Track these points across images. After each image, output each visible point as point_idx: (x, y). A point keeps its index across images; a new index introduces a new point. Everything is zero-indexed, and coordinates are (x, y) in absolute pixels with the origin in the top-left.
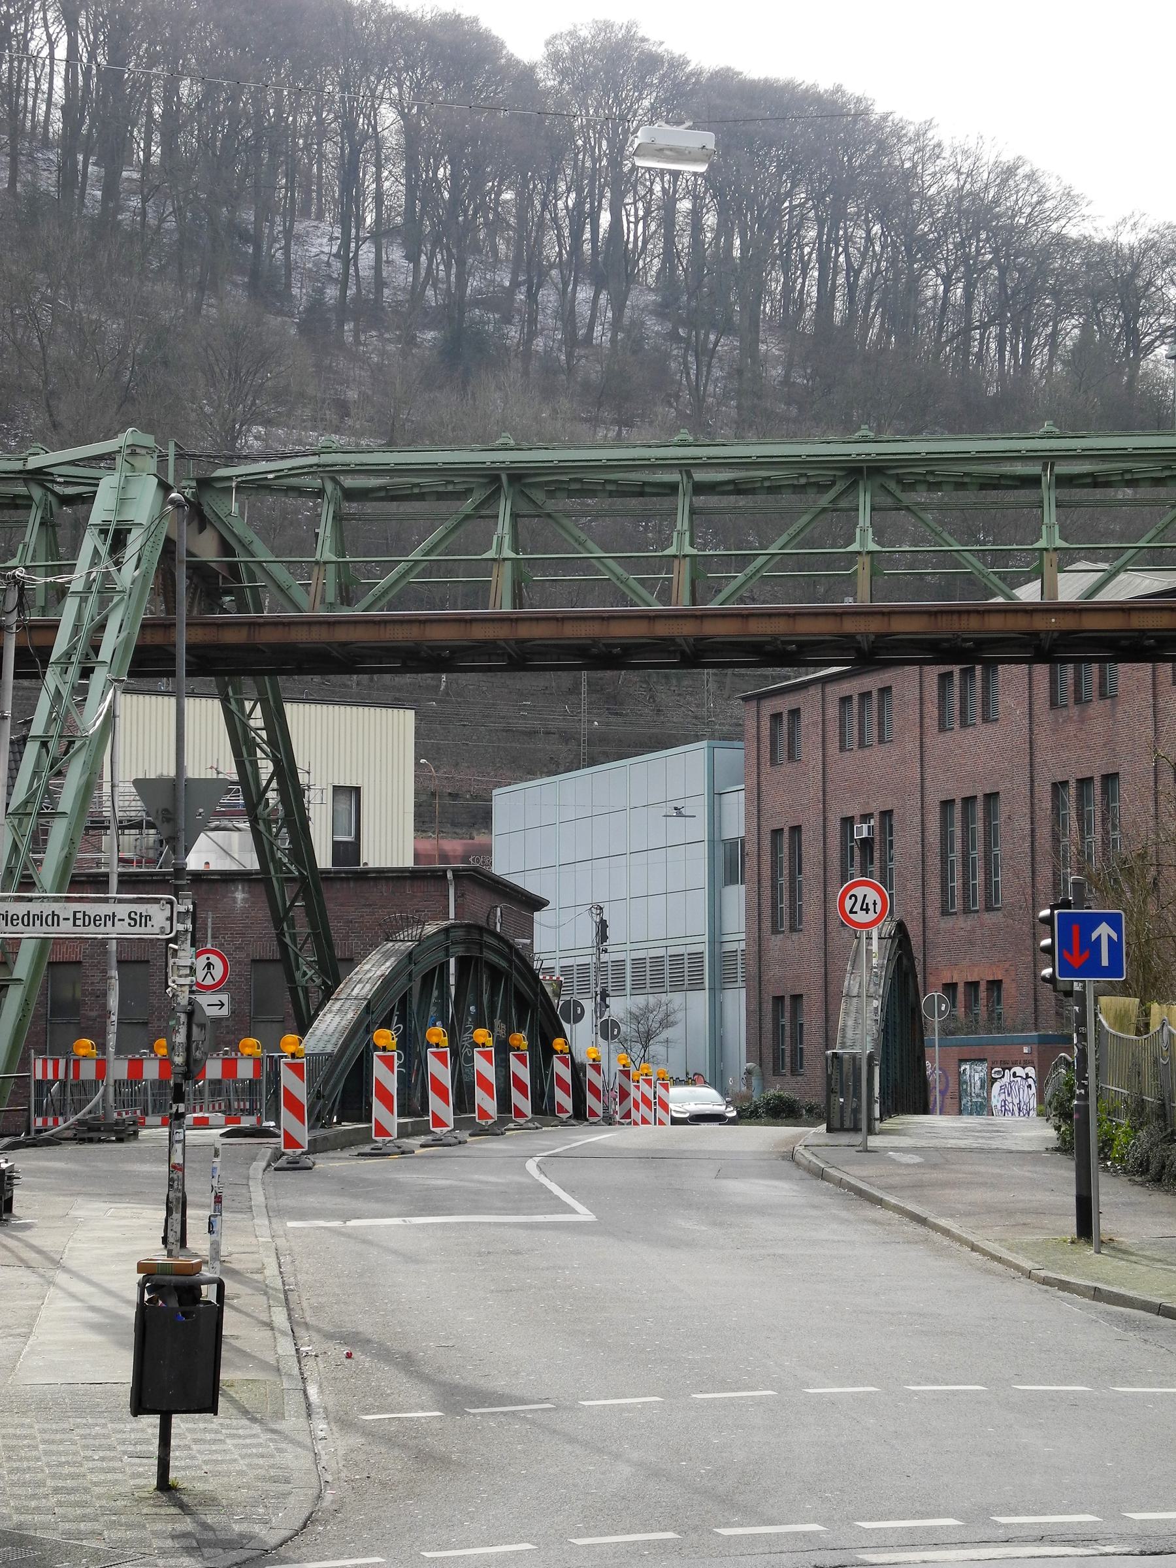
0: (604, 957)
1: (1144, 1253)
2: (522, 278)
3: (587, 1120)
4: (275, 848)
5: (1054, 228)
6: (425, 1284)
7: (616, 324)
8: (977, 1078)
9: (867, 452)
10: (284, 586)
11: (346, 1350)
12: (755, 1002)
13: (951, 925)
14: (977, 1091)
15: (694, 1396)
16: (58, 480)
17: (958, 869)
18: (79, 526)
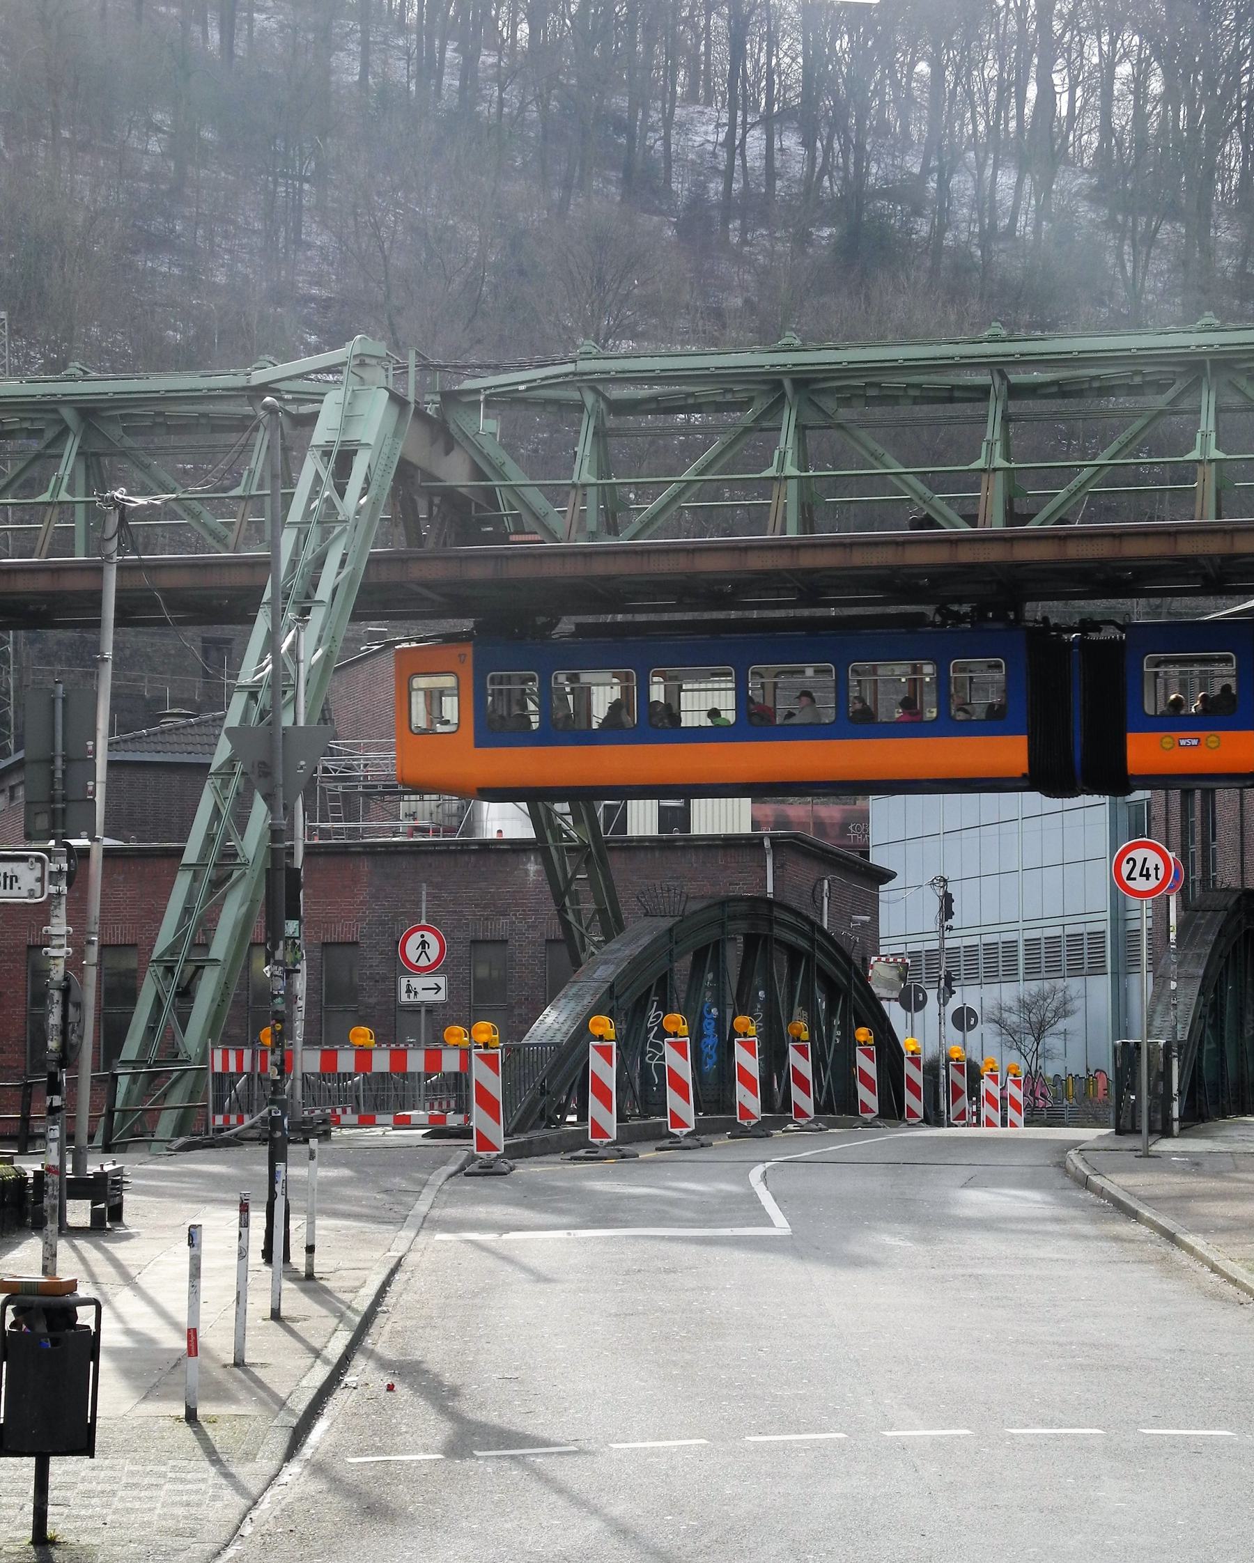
7: (1042, 212)
9: (1209, 343)
15: (747, 1438)
16: (286, 397)
18: (305, 447)
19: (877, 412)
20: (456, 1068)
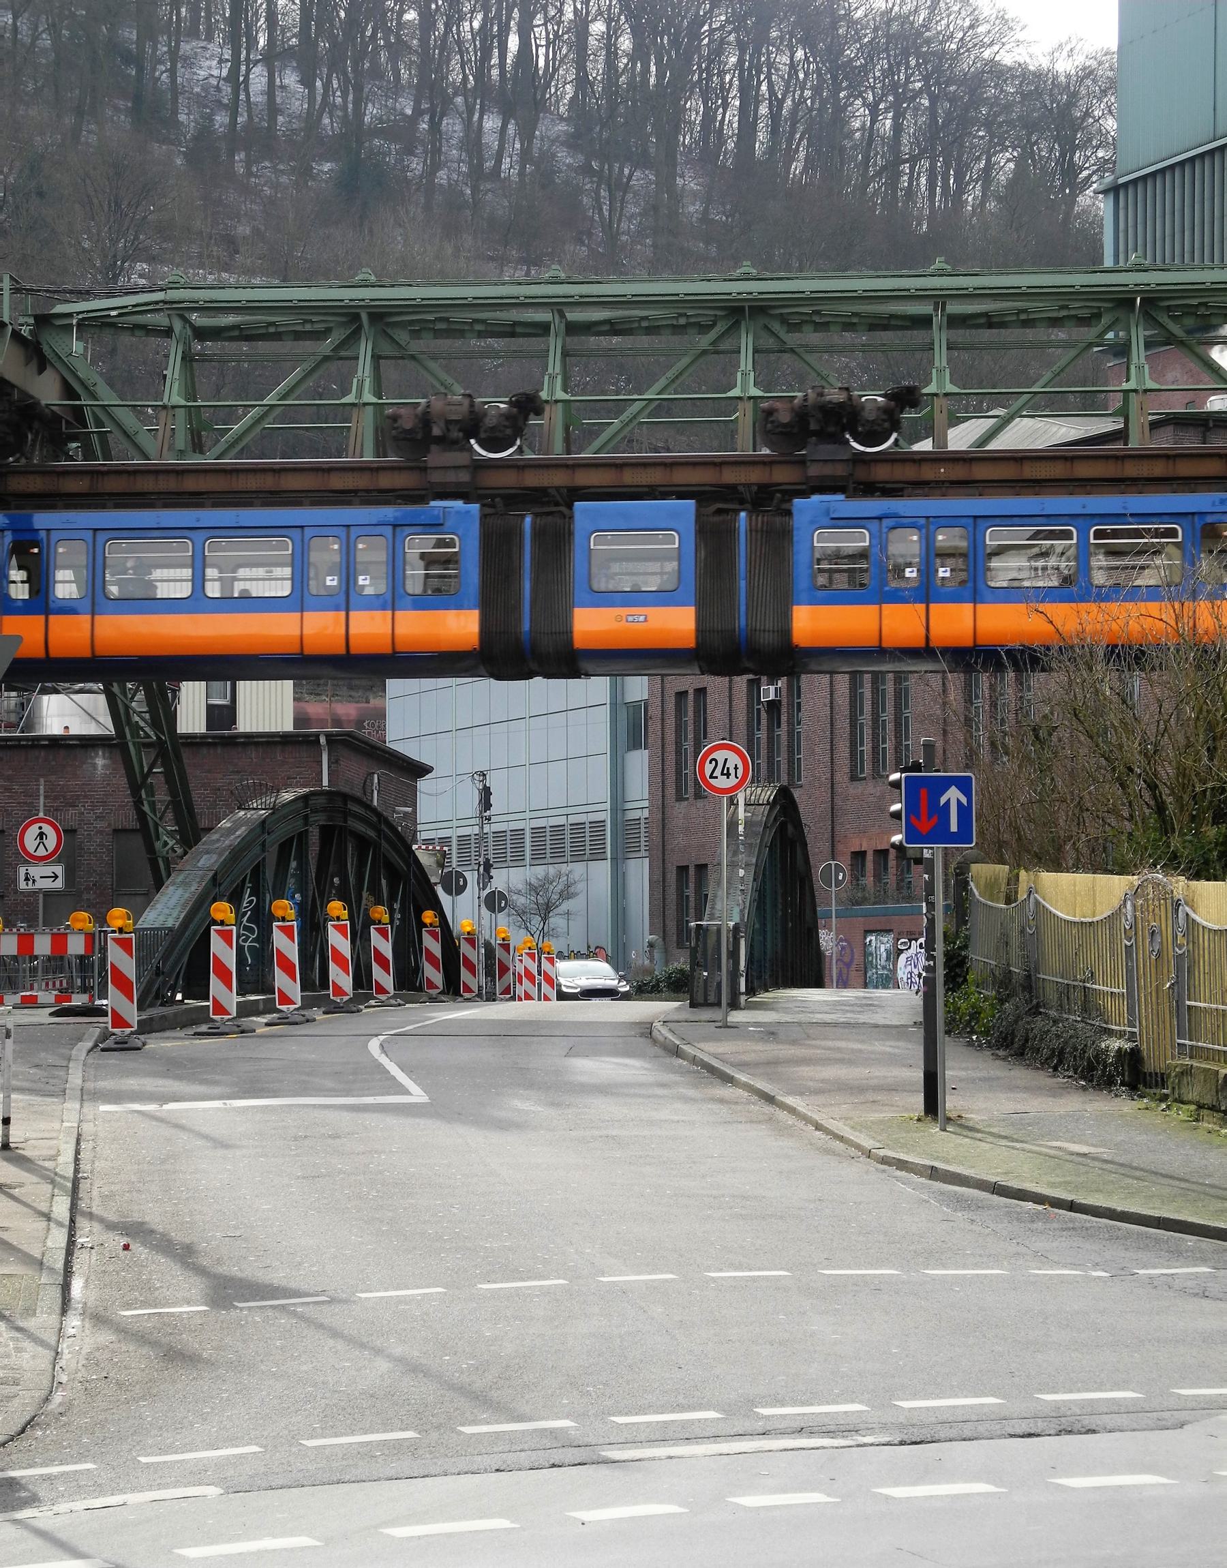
0: (486, 829)
1: (992, 1130)
2: (425, 106)
3: (462, 996)
4: (131, 712)
5: (987, 54)
6: (229, 1170)
7: (525, 155)
8: (883, 949)
9: (748, 290)
10: (131, 431)
11: (124, 1241)
12: (658, 872)
13: (860, 791)
14: (883, 963)
15: (480, 1286)
17: (867, 732)
19: (444, 344)
20: (82, 952)
